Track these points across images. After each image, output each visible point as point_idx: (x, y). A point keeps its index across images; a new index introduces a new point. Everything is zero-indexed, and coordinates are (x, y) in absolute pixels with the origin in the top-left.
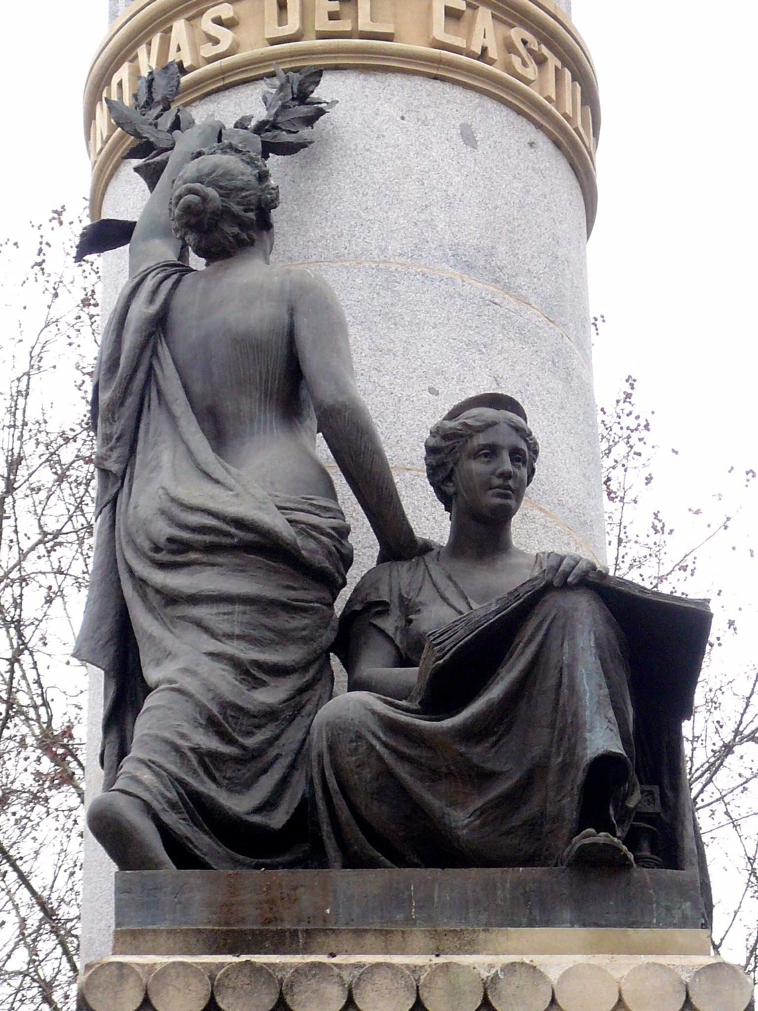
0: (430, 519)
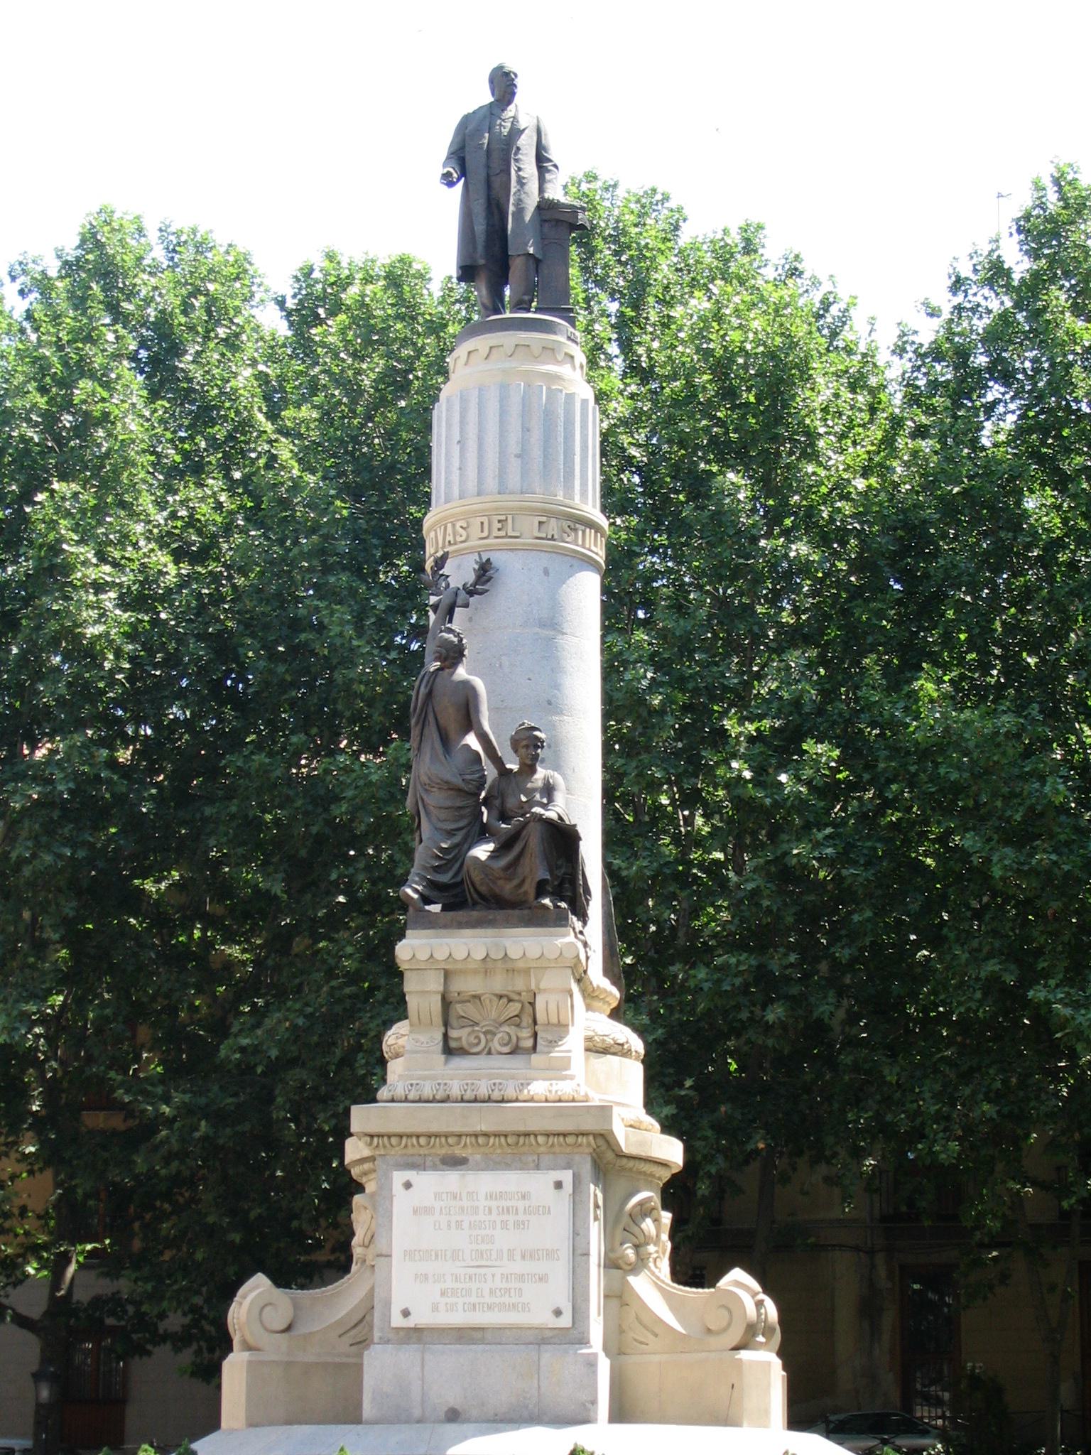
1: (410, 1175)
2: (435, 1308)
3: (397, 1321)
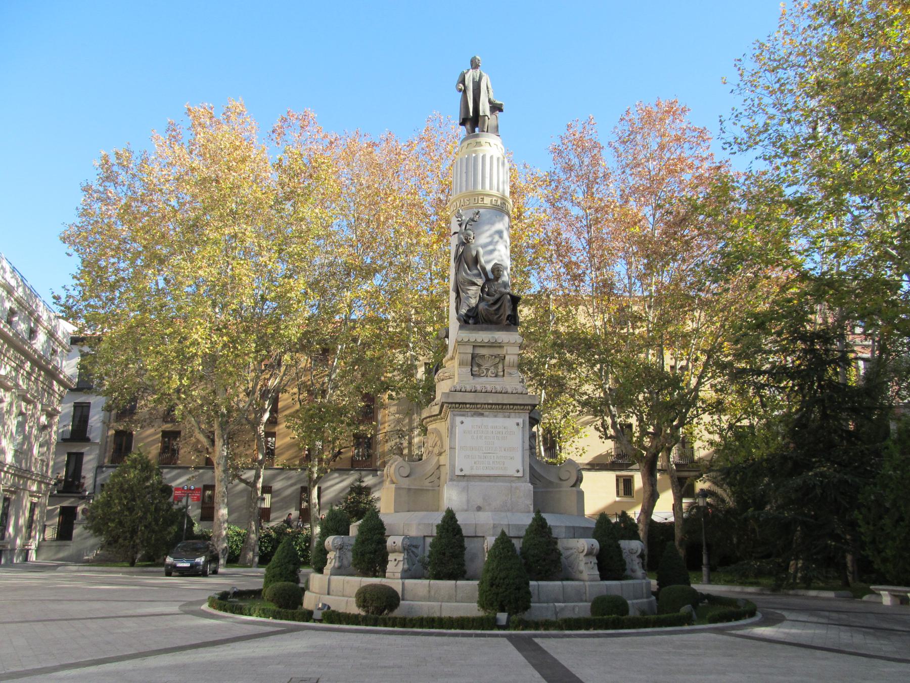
0: (491, 276)
1: (462, 418)
2: (472, 468)
3: (458, 473)
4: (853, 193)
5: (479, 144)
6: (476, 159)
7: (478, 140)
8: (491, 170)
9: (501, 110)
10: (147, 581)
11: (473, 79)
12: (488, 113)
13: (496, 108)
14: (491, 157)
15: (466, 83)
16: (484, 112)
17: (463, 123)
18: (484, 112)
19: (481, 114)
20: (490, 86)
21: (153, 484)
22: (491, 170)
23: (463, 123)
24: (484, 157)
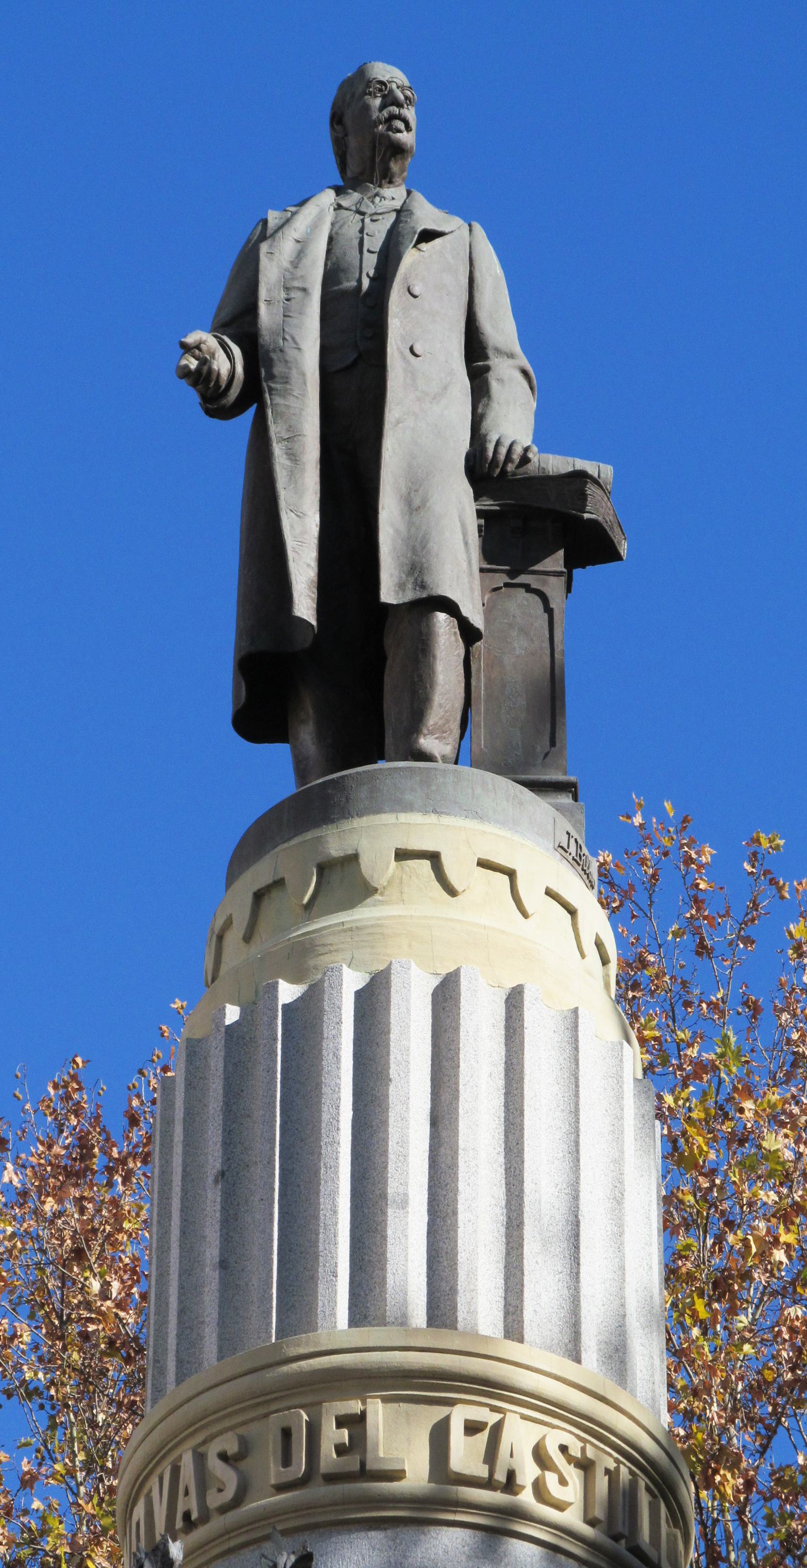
4: (772, 1156)
5: (343, 881)
6: (305, 1020)
7: (336, 841)
8: (442, 1119)
9: (591, 546)
10: (353, 1516)
11: (331, 276)
12: (458, 571)
13: (534, 522)
14: (446, 996)
15: (267, 317)
16: (416, 569)
17: (259, 718)
18: (416, 569)
19: (391, 590)
20: (501, 328)
21: (679, 1234)
22: (442, 1119)
23: (259, 718)
24: (372, 1003)
